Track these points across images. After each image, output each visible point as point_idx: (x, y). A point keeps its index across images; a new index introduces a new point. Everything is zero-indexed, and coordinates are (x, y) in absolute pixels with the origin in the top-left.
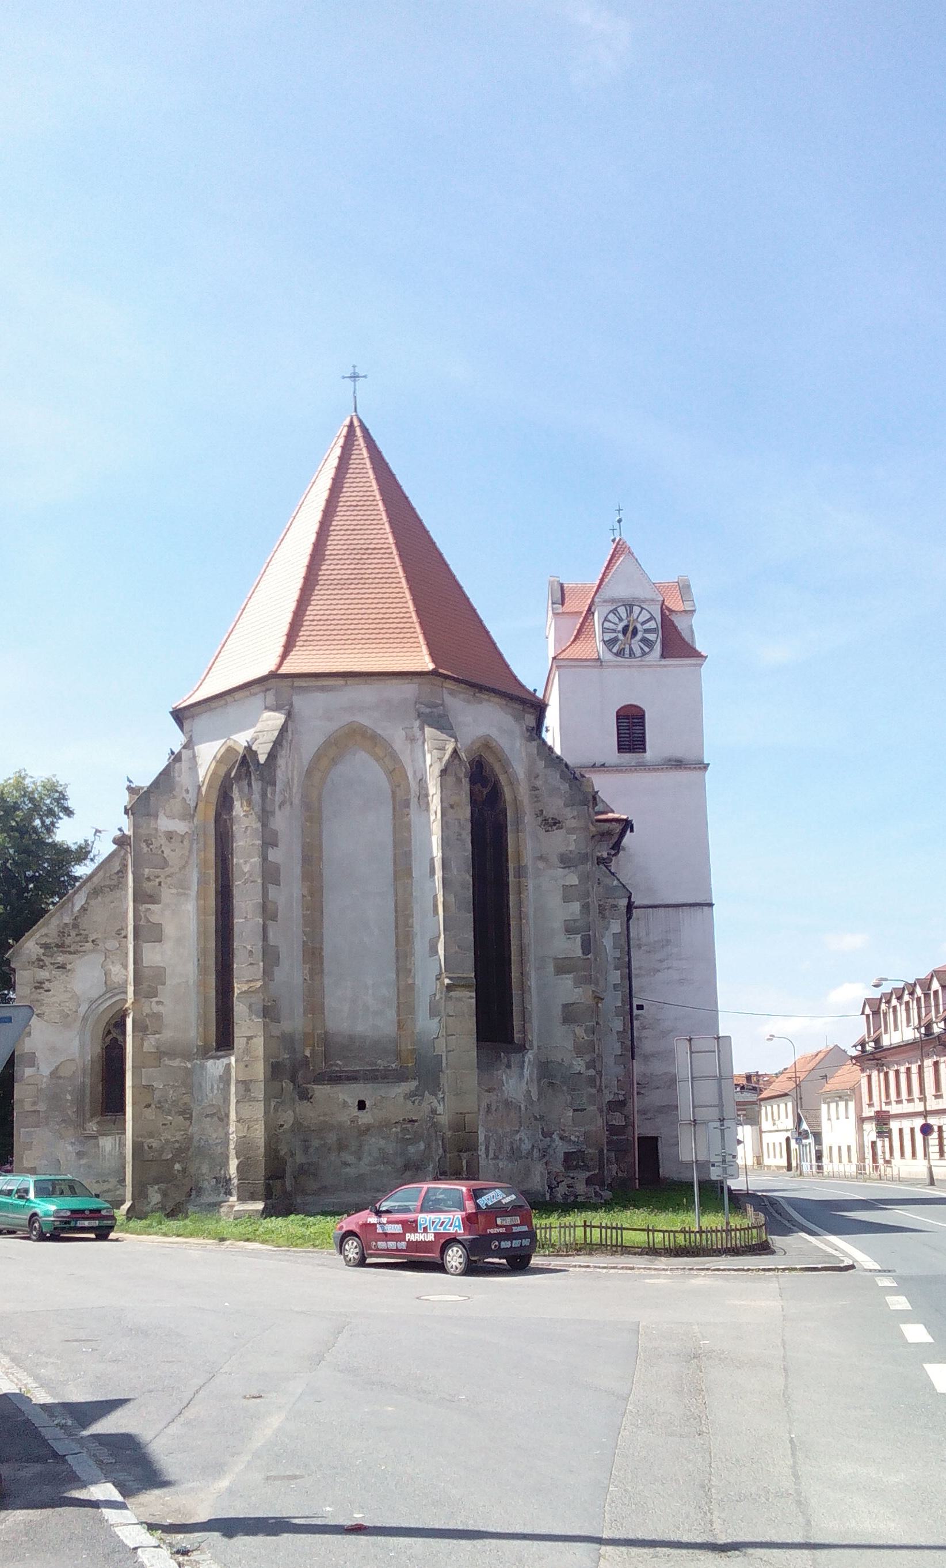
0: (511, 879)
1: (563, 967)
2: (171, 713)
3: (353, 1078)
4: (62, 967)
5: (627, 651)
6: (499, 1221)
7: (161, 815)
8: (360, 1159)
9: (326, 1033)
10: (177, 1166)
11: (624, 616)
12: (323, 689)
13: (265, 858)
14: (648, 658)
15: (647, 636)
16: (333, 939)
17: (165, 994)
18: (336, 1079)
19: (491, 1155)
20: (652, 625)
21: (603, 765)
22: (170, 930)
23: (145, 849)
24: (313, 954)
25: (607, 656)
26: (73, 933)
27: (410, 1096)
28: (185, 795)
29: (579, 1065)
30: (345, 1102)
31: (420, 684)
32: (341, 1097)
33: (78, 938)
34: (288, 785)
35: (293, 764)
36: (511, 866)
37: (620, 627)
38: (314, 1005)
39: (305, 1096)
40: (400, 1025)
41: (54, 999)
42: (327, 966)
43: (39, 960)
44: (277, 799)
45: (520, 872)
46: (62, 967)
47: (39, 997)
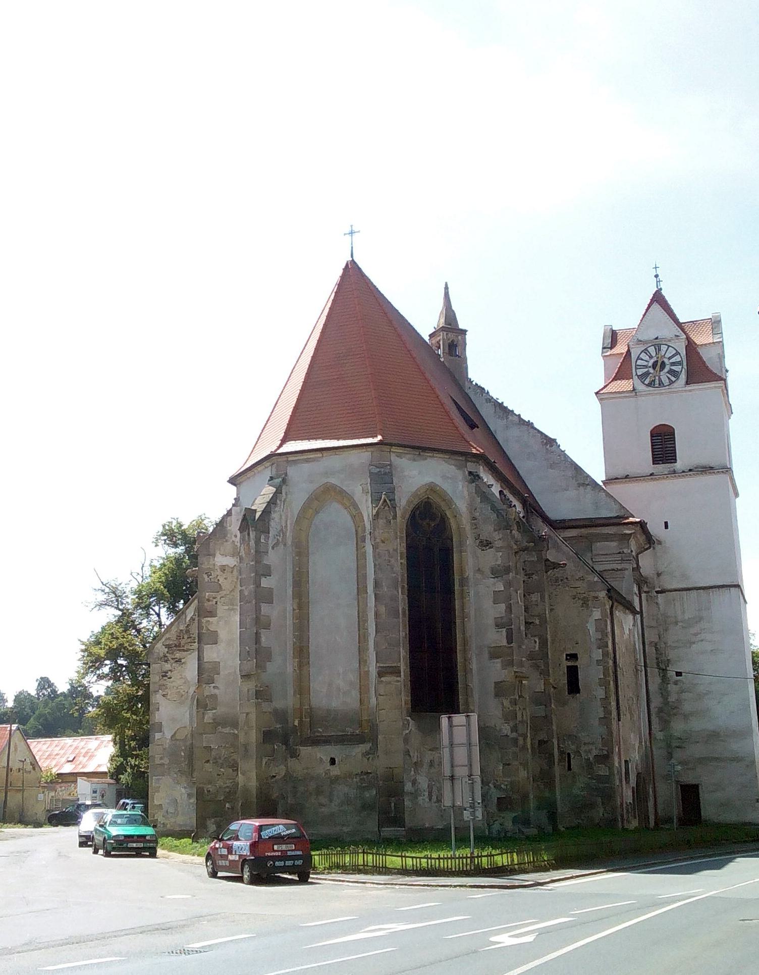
0: (457, 587)
1: (495, 653)
2: (229, 481)
3: (327, 741)
4: (179, 661)
5: (657, 382)
6: (276, 847)
7: (218, 554)
8: (331, 802)
9: (311, 708)
10: (227, 805)
11: (654, 354)
12: (307, 461)
13: (258, 585)
14: (675, 385)
15: (673, 368)
16: (317, 640)
17: (220, 681)
18: (316, 742)
19: (434, 798)
20: (677, 359)
21: (627, 477)
22: (223, 635)
23: (206, 579)
24: (302, 652)
25: (641, 387)
26: (186, 637)
27: (366, 754)
28: (234, 539)
29: (506, 729)
30: (321, 759)
31: (372, 452)
32: (319, 755)
33: (189, 640)
34: (282, 532)
35: (287, 516)
36: (457, 577)
37: (650, 364)
38: (302, 688)
39: (294, 755)
40: (361, 702)
41: (174, 684)
42: (312, 659)
43: (165, 656)
44: (270, 542)
45: (464, 581)
46: (179, 661)
47: (165, 683)
